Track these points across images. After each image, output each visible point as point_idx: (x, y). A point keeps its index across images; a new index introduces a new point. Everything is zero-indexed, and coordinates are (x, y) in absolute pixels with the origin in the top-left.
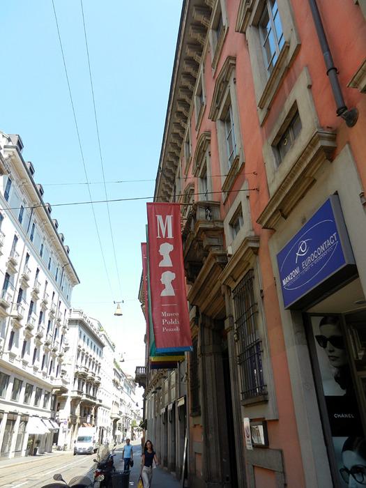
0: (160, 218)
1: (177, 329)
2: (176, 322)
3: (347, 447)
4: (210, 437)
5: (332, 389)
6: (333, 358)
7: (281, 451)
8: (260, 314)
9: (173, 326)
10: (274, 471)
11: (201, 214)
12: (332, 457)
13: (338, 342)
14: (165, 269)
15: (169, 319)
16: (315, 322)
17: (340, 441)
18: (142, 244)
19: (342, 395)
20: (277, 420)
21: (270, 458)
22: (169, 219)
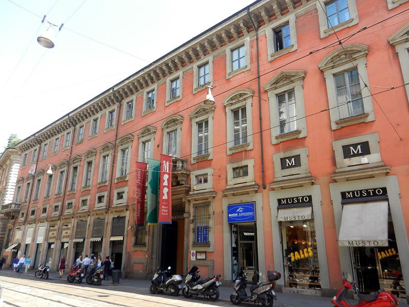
0: (164, 162)
1: (167, 214)
2: (167, 211)
3: (235, 259)
4: (153, 256)
5: (234, 245)
6: (235, 237)
7: (214, 261)
8: (211, 219)
9: (165, 213)
10: (208, 266)
11: (179, 164)
12: (232, 262)
13: (236, 232)
14: (165, 186)
15: (164, 209)
16: (233, 226)
17: (234, 258)
18: (403, 280)
19: (366, 254)
20: (213, 252)
21: (208, 263)
22: (168, 163)
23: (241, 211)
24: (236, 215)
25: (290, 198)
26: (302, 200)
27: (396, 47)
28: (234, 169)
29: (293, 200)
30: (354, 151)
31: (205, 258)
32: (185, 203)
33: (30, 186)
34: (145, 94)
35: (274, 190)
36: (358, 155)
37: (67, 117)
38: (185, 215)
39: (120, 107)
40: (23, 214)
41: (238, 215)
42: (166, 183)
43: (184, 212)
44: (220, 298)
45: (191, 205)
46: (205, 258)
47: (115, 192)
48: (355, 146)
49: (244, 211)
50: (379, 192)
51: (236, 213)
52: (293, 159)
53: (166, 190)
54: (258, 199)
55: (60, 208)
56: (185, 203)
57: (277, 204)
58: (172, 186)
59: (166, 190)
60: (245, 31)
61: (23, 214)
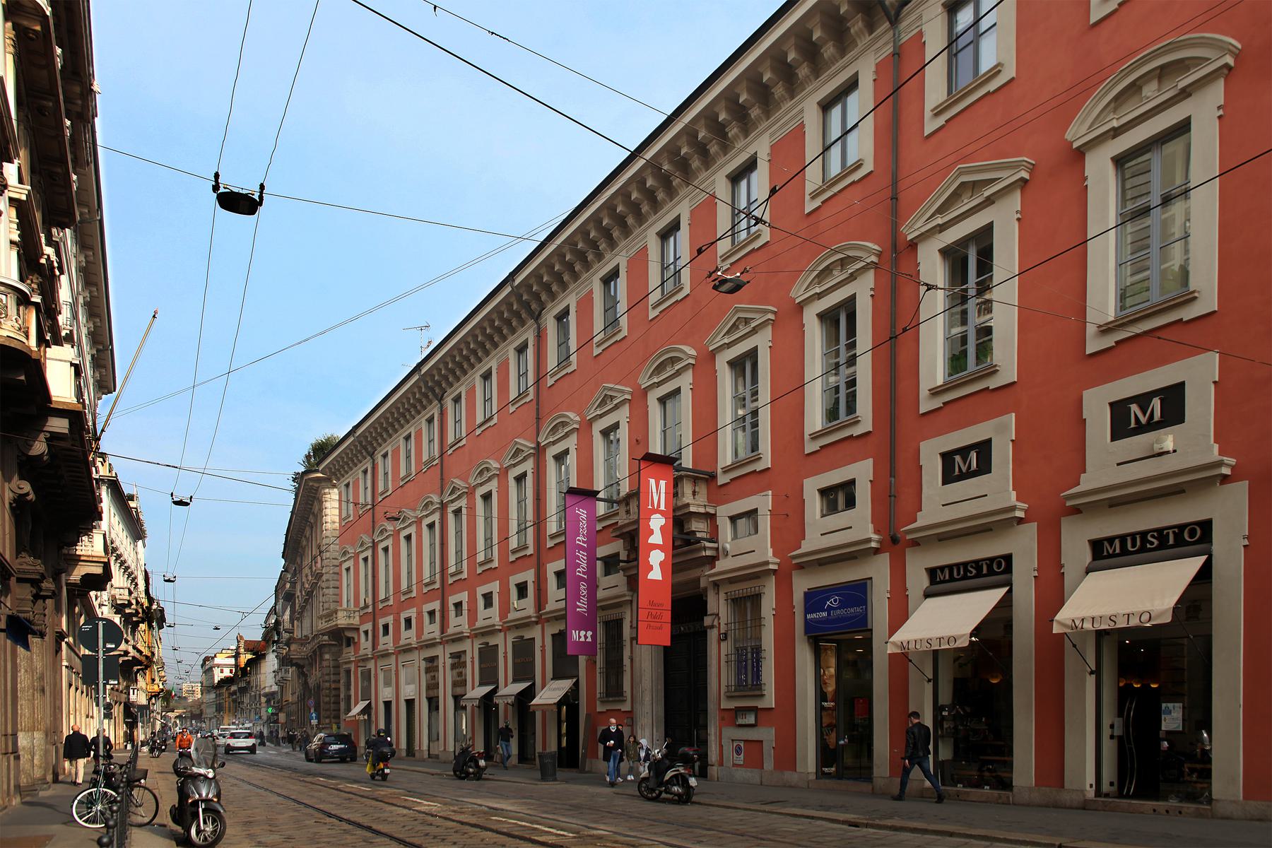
14: (656, 547)
23: (835, 605)
24: (825, 614)
25: (1133, 535)
26: (990, 567)
27: (1087, 155)
28: (824, 492)
29: (966, 570)
30: (962, 465)
31: (754, 722)
32: (706, 589)
33: (464, 518)
34: (721, 187)
35: (918, 544)
36: (1152, 426)
37: (508, 290)
38: (707, 621)
39: (540, 336)
40: (366, 632)
41: (829, 614)
42: (656, 538)
43: (704, 612)
44: (694, 799)
45: (722, 596)
46: (754, 722)
47: (812, 487)
48: (1143, 400)
49: (843, 605)
50: (999, 565)
51: (823, 610)
52: (973, 455)
53: (656, 557)
54: (879, 572)
55: (465, 606)
56: (706, 589)
57: (1087, 557)
58: (674, 547)
59: (656, 557)
60: (856, 25)
61: (366, 632)
